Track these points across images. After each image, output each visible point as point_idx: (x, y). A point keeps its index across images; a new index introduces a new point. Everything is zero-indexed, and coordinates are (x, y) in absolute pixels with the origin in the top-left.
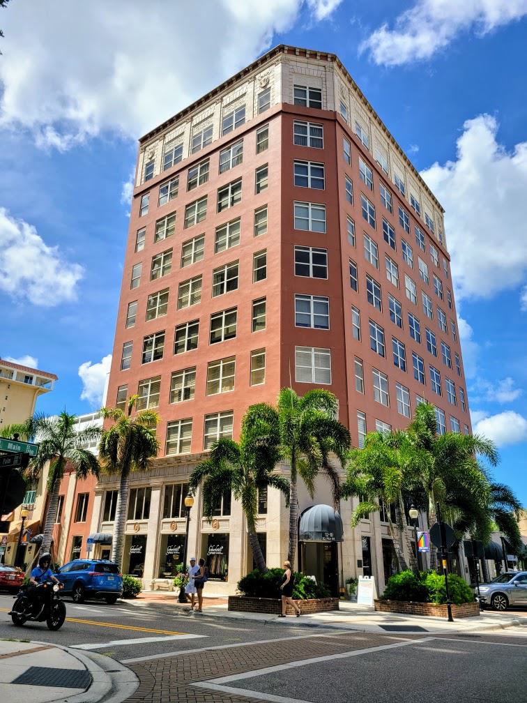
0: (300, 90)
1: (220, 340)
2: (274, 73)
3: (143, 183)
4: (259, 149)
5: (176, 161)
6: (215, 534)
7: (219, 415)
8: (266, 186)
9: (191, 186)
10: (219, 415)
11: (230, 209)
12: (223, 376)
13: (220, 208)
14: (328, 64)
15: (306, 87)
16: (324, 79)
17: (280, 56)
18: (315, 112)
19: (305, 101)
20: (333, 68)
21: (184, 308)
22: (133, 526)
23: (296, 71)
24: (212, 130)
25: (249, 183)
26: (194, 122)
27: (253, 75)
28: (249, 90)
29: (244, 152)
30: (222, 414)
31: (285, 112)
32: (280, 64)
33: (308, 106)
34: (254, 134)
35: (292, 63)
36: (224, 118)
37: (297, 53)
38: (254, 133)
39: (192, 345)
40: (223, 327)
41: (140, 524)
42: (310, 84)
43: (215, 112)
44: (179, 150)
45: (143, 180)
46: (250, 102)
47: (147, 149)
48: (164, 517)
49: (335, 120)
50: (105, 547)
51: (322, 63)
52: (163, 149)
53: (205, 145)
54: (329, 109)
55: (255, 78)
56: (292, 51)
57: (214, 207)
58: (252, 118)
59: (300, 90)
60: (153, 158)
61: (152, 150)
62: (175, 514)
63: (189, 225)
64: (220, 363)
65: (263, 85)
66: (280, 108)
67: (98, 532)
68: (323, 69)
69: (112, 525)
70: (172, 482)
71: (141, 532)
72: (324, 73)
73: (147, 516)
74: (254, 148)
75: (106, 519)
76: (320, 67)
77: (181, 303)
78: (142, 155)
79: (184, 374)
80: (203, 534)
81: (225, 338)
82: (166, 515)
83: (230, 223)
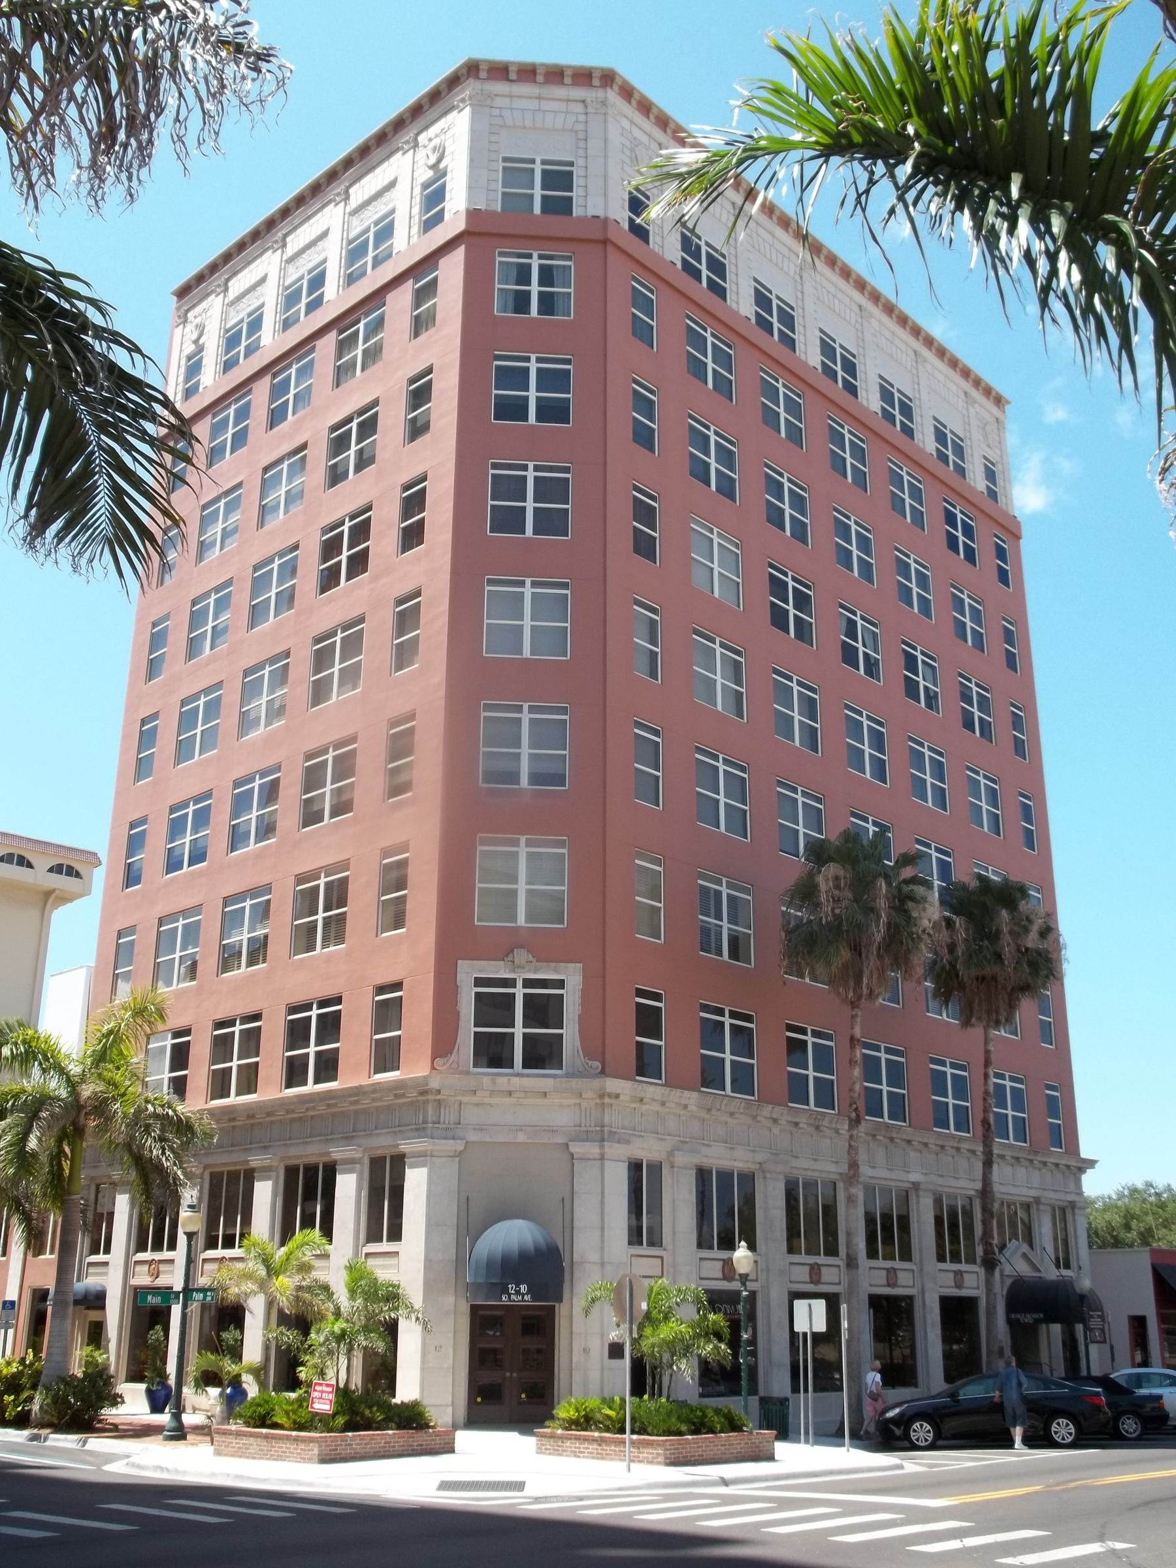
0: (517, 171)
2: (454, 131)
3: (414, 239)
4: (420, 325)
5: (313, 306)
7: (315, 1006)
15: (533, 161)
16: (581, 135)
17: (469, 88)
19: (532, 196)
20: (604, 103)
21: (252, 735)
22: (145, 1268)
23: (509, 122)
24: (392, 223)
25: (393, 419)
26: (291, 249)
28: (403, 170)
31: (478, 234)
32: (468, 110)
33: (537, 209)
35: (499, 102)
36: (350, 242)
37: (513, 76)
38: (409, 287)
41: (161, 1261)
42: (545, 151)
44: (385, 231)
45: (415, 230)
46: (405, 205)
47: (190, 315)
49: (605, 242)
50: (93, 1315)
51: (579, 93)
52: (224, 319)
53: (377, 262)
54: (591, 212)
55: (416, 140)
56: (500, 71)
58: (408, 244)
59: (517, 171)
60: (442, 166)
61: (436, 142)
63: (268, 518)
65: (432, 160)
66: (461, 226)
68: (579, 108)
69: (172, 1261)
70: (300, 1157)
72: (582, 118)
73: (396, 1234)
74: (406, 323)
75: (374, 1236)
77: (246, 723)
78: (178, 331)
82: (141, 1247)
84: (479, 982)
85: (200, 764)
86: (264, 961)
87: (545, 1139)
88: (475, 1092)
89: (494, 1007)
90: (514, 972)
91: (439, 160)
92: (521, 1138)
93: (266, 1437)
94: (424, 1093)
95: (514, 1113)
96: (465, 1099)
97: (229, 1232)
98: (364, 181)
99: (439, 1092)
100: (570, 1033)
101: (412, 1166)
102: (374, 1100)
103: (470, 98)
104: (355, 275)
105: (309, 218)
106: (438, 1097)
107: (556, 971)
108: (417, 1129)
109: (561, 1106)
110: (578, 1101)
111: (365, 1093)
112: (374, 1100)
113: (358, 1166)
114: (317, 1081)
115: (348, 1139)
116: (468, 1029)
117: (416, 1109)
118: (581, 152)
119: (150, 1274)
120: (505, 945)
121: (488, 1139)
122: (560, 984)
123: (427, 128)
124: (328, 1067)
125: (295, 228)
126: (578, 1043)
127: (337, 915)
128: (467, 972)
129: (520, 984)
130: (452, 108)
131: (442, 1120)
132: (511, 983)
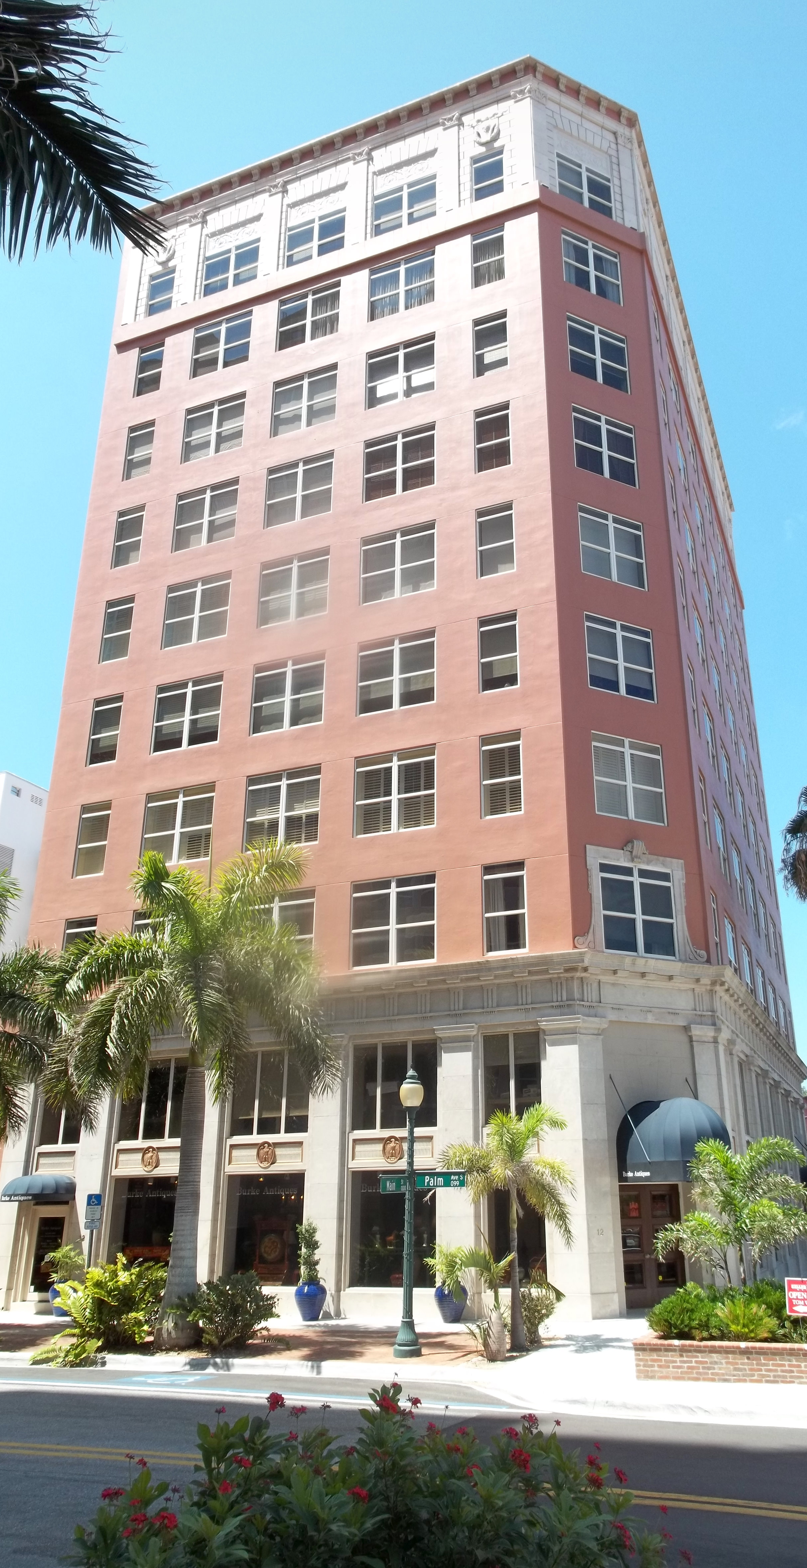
0: (568, 170)
1: (390, 706)
6: (266, 1176)
8: (503, 362)
9: (201, 366)
10: (393, 884)
11: (402, 402)
12: (182, 827)
13: (189, 450)
14: (623, 130)
17: (528, 84)
18: (597, 220)
27: (280, 181)
29: (165, 369)
30: (401, 882)
34: (188, 337)
39: (203, 734)
40: (187, 717)
41: (160, 1149)
42: (592, 163)
43: (350, 187)
48: (42, 1143)
51: (611, 124)
52: (283, 216)
56: (553, 79)
57: (359, 393)
58: (456, 206)
59: (568, 170)
60: (171, 264)
61: (492, 123)
62: (154, 1131)
64: (177, 797)
65: (486, 137)
66: (533, 194)
67: (26, 1172)
68: (611, 137)
70: (379, 1036)
71: (285, 1164)
76: (606, 133)
79: (284, 783)
80: (353, 1172)
81: (192, 742)
83: (404, 436)
84: (604, 868)
85: (195, 647)
86: (206, 855)
87: (670, 1021)
88: (615, 972)
89: (617, 893)
90: (633, 861)
91: (495, 139)
92: (650, 1019)
93: (746, 1352)
94: (574, 969)
95: (644, 994)
96: (603, 978)
97: (295, 1113)
98: (390, 148)
99: (585, 969)
100: (679, 922)
101: (553, 1044)
102: (496, 977)
103: (529, 92)
104: (382, 227)
105: (318, 171)
106: (584, 975)
107: (664, 865)
108: (557, 1007)
109: (680, 990)
110: (693, 986)
111: (490, 970)
112: (496, 977)
113: (472, 1044)
114: (401, 958)
115: (456, 1016)
116: (599, 913)
117: (559, 985)
118: (615, 174)
119: (261, 1158)
120: (626, 837)
121: (624, 1019)
122: (665, 877)
123: (474, 110)
124: (419, 943)
125: (300, 178)
126: (687, 933)
127: (426, 796)
128: (596, 856)
129: (636, 873)
130: (508, 97)
131: (586, 999)
132: (628, 871)
